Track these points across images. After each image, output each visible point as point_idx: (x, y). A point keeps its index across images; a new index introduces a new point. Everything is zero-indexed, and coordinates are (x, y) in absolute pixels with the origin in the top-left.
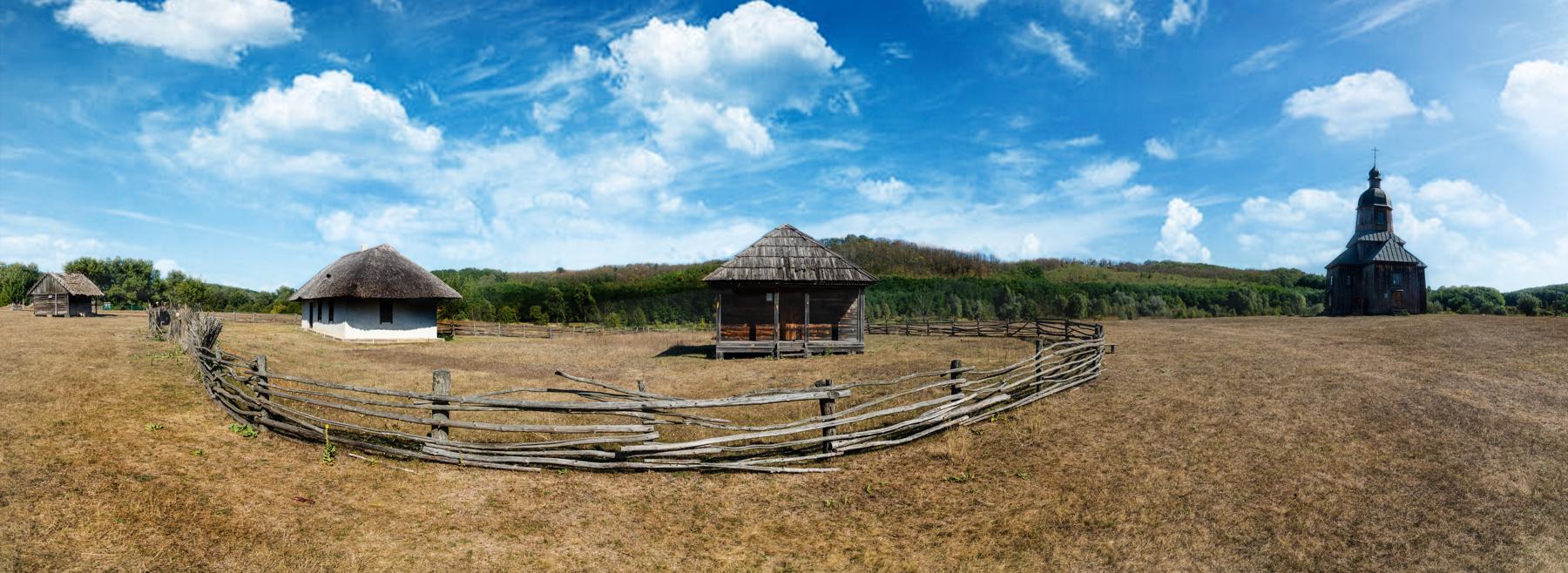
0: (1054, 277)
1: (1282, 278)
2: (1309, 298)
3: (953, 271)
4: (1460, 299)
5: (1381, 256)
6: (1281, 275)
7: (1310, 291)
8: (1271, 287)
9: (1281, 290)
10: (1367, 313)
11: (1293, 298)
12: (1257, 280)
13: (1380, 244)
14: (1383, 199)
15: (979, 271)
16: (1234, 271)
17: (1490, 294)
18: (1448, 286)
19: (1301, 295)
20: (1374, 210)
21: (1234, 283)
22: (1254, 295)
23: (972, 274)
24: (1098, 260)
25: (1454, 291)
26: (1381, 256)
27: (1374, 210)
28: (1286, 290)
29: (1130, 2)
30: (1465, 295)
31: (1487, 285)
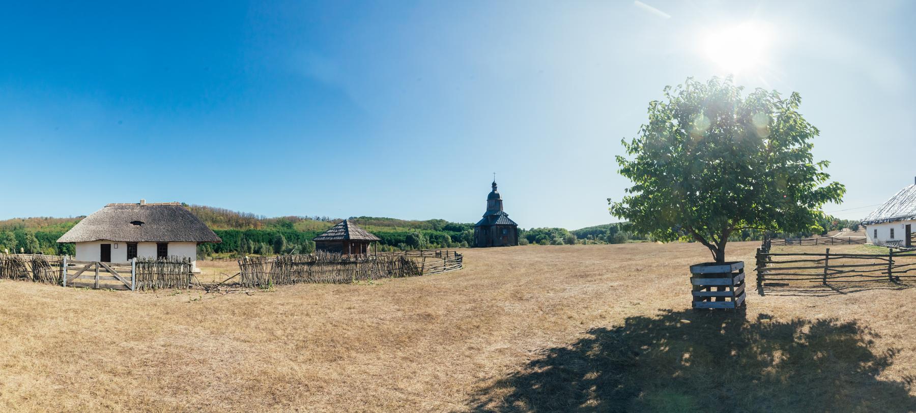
0: (297, 227)
1: (435, 225)
2: (452, 237)
3: (241, 226)
4: (543, 236)
5: (499, 222)
6: (434, 224)
7: (452, 233)
8: (429, 231)
9: (435, 233)
10: (493, 246)
11: (444, 237)
12: (420, 227)
13: (498, 217)
14: (498, 195)
15: (255, 225)
16: (404, 222)
17: (561, 232)
18: (536, 228)
19: (448, 235)
20: (494, 200)
21: (406, 230)
22: (421, 236)
23: (252, 227)
24: (321, 217)
25: (540, 231)
26: (499, 222)
27: (494, 200)
28: (439, 233)
29: (159, 411)
30: (546, 233)
31: (559, 227)
